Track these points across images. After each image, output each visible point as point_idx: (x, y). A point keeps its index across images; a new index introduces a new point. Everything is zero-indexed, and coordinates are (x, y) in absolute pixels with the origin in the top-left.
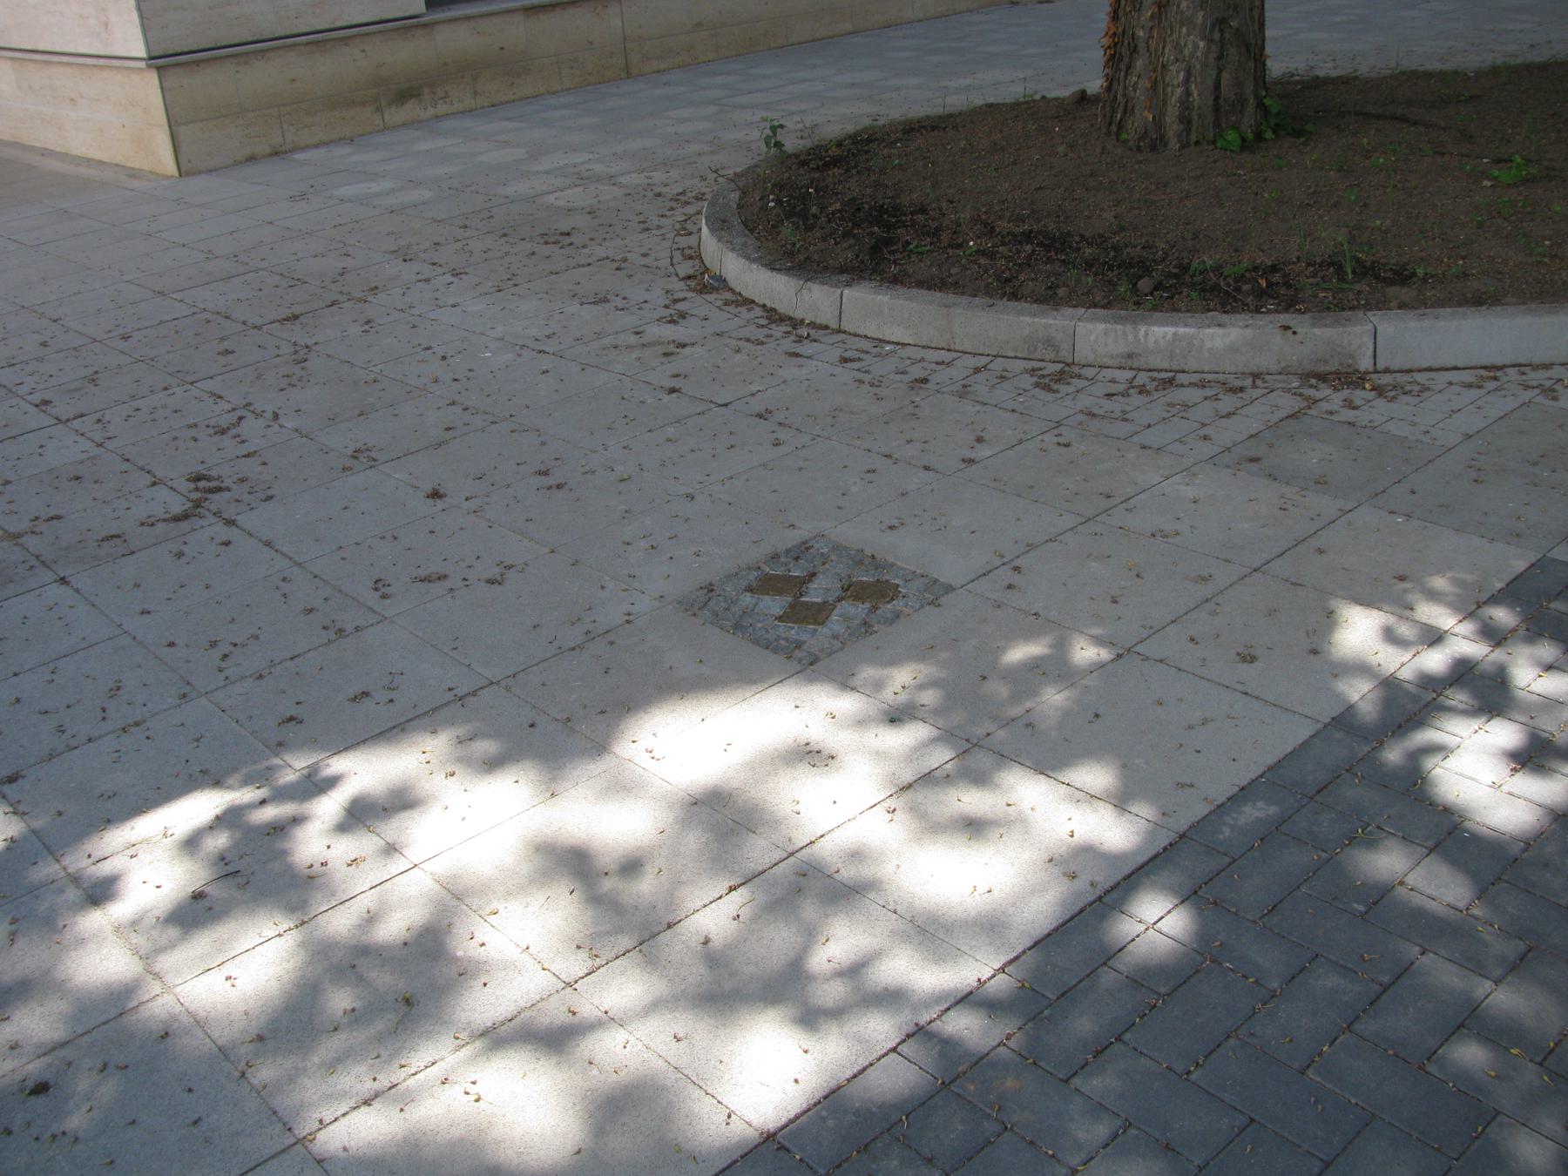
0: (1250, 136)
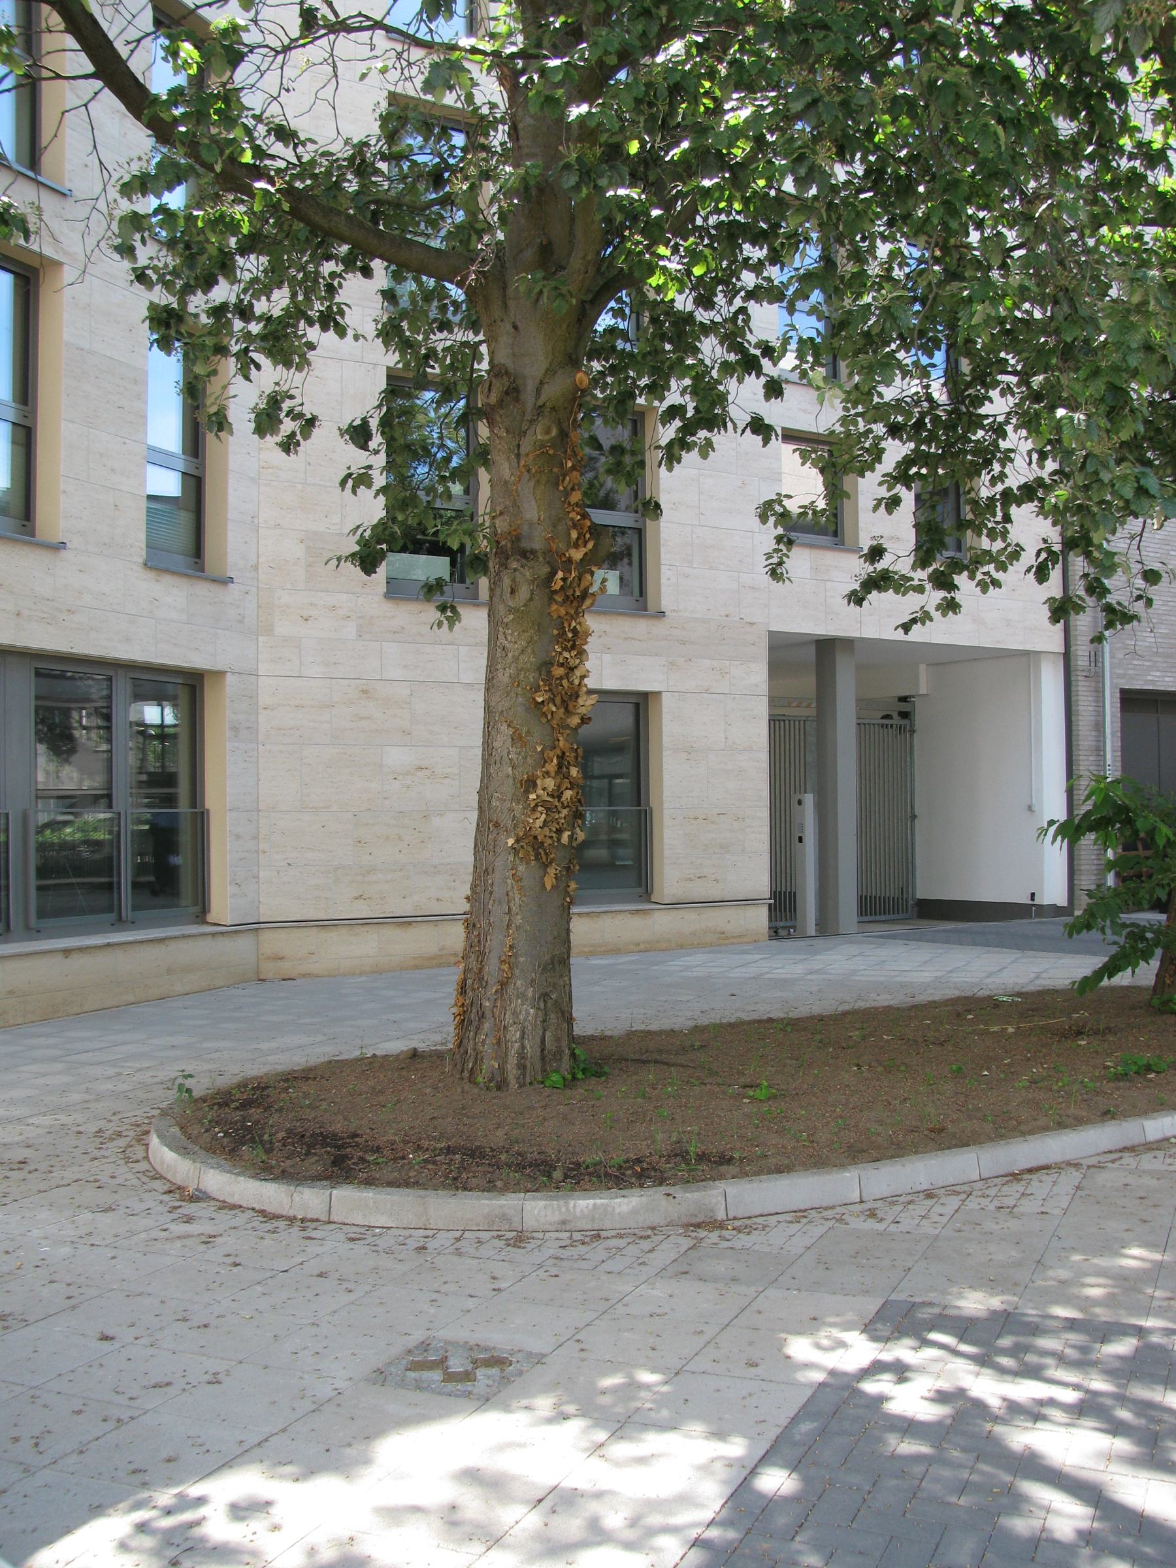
0: (569, 1077)
